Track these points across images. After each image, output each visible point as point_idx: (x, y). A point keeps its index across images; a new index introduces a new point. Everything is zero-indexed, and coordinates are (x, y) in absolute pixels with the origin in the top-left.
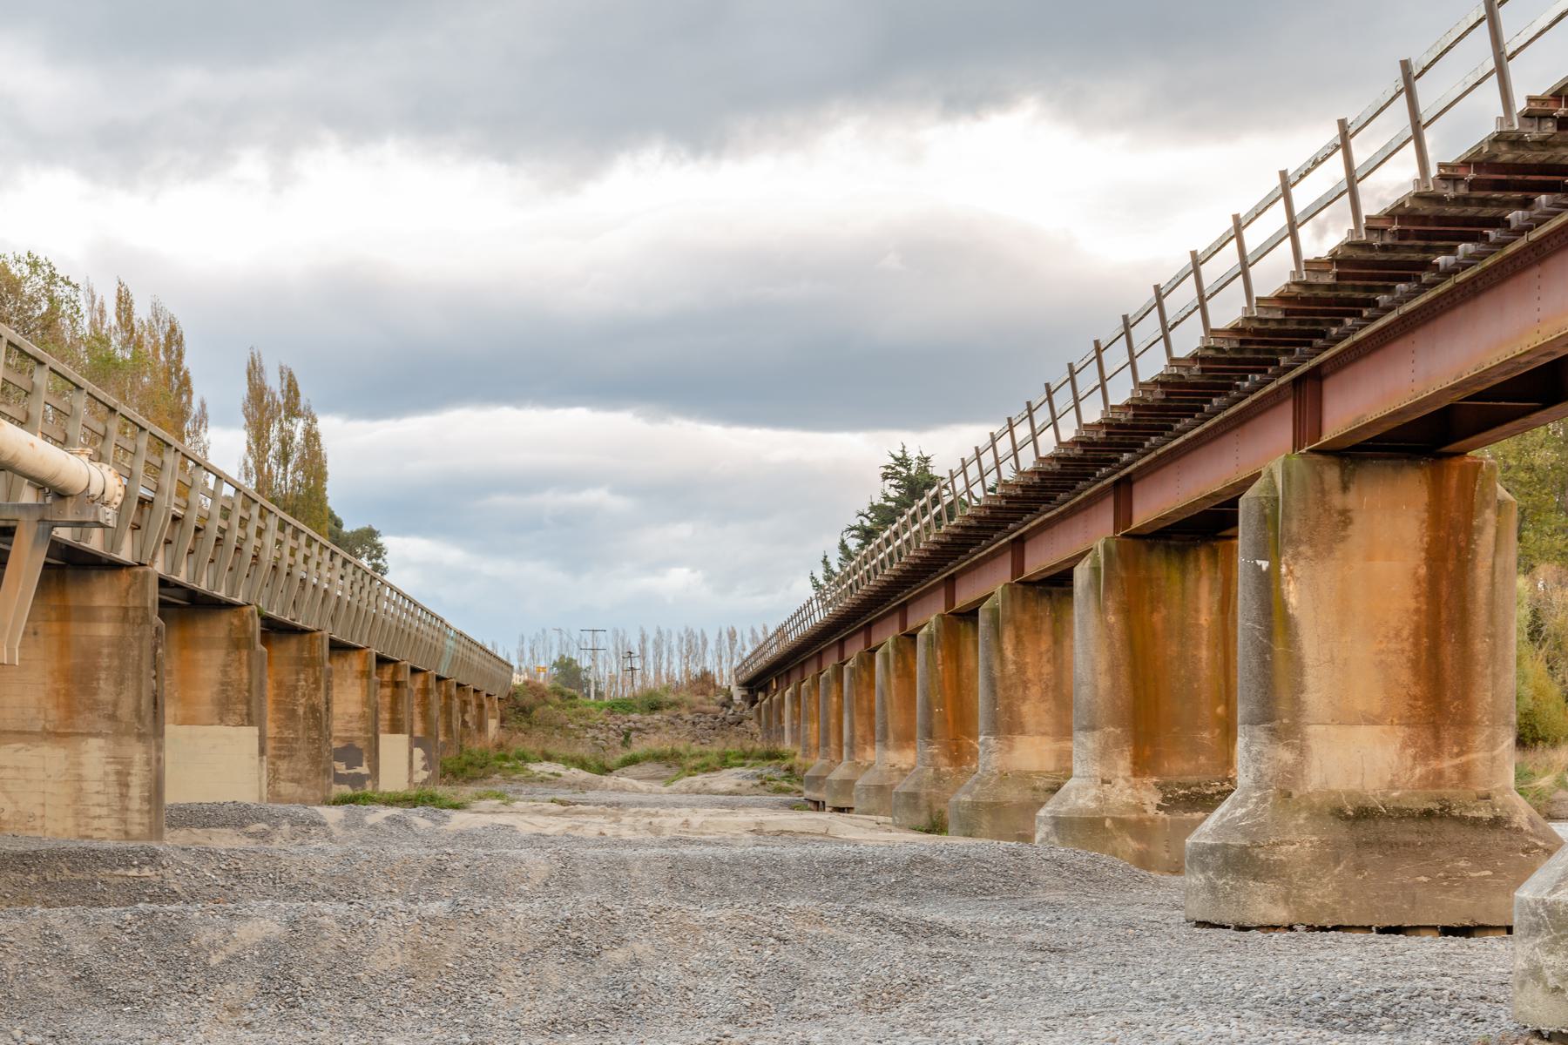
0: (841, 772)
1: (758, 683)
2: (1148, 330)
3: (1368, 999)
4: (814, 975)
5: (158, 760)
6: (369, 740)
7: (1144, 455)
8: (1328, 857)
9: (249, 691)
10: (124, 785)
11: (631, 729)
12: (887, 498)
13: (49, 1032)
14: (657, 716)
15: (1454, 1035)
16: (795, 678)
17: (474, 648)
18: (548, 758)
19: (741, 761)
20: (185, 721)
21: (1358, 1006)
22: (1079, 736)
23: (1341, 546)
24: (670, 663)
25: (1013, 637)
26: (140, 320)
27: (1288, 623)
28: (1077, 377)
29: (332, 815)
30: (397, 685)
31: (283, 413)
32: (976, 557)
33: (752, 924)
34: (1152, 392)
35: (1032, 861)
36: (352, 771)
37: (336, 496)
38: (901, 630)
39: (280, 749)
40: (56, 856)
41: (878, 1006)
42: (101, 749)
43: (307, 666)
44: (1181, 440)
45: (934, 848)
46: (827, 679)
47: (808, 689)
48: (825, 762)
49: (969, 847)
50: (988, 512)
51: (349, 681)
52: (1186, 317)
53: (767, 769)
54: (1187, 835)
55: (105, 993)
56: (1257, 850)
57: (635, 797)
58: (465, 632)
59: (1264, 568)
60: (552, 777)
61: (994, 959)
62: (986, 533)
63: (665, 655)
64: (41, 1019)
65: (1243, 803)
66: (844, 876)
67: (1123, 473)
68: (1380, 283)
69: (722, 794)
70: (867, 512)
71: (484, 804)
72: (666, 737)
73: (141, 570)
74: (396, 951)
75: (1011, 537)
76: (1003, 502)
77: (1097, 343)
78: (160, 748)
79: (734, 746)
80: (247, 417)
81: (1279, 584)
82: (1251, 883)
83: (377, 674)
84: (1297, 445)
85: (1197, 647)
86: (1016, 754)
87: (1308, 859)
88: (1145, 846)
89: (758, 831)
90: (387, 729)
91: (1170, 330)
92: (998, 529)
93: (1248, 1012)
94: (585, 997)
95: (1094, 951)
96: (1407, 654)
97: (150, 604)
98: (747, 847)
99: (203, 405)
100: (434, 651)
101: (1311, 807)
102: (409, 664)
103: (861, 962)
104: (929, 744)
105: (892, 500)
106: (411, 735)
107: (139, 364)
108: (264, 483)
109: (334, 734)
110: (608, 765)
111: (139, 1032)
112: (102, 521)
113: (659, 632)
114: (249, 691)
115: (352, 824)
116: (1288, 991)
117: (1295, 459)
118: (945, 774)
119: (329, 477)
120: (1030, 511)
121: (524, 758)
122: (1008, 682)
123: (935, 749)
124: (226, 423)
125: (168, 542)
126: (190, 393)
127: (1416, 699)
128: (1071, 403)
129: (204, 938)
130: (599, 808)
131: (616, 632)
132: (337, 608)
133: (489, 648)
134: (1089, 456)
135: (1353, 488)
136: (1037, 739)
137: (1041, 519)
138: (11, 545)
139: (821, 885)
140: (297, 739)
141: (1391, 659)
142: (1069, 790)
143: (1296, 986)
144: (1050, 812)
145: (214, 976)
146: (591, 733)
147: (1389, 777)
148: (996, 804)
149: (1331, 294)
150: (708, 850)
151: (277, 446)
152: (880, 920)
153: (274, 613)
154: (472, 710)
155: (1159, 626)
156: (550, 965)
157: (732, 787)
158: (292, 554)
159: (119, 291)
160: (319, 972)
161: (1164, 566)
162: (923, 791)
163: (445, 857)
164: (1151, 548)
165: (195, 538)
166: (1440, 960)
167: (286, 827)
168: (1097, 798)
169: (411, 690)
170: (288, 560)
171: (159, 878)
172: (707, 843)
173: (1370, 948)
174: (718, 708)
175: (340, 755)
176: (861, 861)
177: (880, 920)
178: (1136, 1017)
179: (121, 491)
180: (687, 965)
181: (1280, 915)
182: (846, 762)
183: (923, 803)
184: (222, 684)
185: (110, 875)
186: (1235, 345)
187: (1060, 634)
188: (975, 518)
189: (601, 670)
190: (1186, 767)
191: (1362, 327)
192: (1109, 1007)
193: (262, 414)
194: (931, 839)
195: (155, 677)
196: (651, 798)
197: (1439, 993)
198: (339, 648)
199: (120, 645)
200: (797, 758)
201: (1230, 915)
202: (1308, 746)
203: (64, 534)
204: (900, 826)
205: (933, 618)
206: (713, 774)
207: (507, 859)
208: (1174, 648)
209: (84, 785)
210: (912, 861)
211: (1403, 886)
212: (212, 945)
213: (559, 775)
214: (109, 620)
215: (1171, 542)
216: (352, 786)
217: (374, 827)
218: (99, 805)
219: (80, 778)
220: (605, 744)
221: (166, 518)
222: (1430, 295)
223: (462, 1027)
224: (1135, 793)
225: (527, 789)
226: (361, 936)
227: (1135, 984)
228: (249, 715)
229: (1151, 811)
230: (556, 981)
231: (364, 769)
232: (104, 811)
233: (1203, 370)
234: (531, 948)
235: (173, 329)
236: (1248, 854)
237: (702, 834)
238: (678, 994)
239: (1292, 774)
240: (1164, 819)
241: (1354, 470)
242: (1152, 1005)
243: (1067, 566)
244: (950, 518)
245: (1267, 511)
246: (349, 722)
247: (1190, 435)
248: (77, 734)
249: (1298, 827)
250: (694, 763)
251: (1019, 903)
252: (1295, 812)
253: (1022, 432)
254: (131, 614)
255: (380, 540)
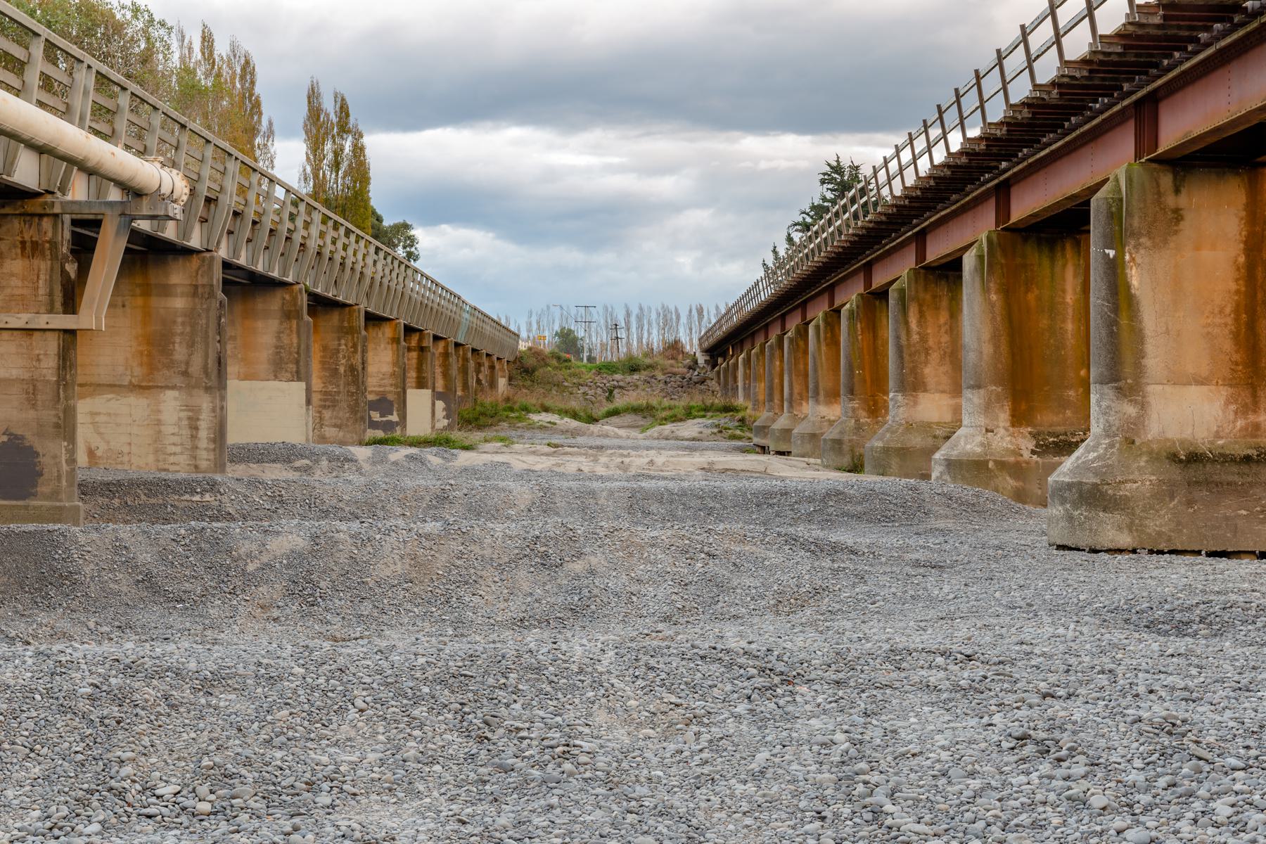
0: (782, 422)
1: (719, 349)
2: (1016, 60)
3: (1189, 609)
4: (736, 583)
5: (222, 408)
6: (398, 394)
7: (1018, 163)
8: (1165, 492)
9: (298, 353)
10: (195, 428)
11: (615, 387)
12: (824, 199)
13: (117, 623)
14: (636, 376)
15: (1258, 639)
16: (747, 346)
17: (486, 319)
18: (546, 410)
19: (702, 413)
20: (247, 377)
21: (1180, 615)
22: (968, 394)
23: (1174, 238)
24: (649, 334)
25: (916, 312)
26: (220, 55)
27: (1131, 302)
28: (962, 100)
29: (362, 453)
30: (422, 349)
31: (335, 130)
32: (887, 247)
33: (687, 542)
34: (1021, 112)
35: (927, 495)
36: (384, 419)
37: (378, 198)
38: (830, 307)
39: (325, 400)
40: (134, 484)
41: (786, 609)
42: (176, 399)
43: (347, 333)
44: (1047, 151)
45: (846, 484)
46: (771, 347)
47: (757, 355)
48: (771, 414)
49: (875, 483)
50: (895, 210)
51: (382, 346)
52: (1046, 51)
53: (723, 420)
54: (1049, 475)
55: (162, 593)
56: (1106, 487)
57: (616, 442)
58: (478, 307)
59: (1111, 256)
60: (549, 425)
61: (885, 573)
62: (895, 227)
63: (646, 327)
64: (111, 613)
65: (1095, 448)
66: (771, 505)
67: (1001, 178)
68: (1200, 24)
69: (687, 440)
70: (808, 210)
71: (488, 446)
72: (643, 393)
73: (208, 255)
74: (397, 561)
75: (914, 231)
76: (907, 202)
77: (977, 72)
78: (223, 398)
79: (697, 401)
80: (306, 132)
81: (1124, 268)
82: (1101, 514)
83: (405, 340)
84: (1138, 155)
85: (1064, 321)
86: (920, 408)
87: (1148, 495)
88: (1021, 483)
89: (708, 469)
90: (414, 385)
91: (1034, 61)
92: (903, 224)
93: (1087, 618)
94: (549, 599)
95: (968, 567)
96: (1229, 327)
97: (215, 282)
98: (698, 481)
99: (271, 124)
100: (453, 322)
101: (1150, 453)
102: (432, 333)
103: (775, 574)
104: (851, 400)
105: (828, 201)
106: (433, 390)
107: (219, 90)
108: (319, 186)
109: (369, 389)
110: (595, 416)
111: (188, 624)
112: (171, 214)
113: (641, 309)
114: (298, 353)
115: (375, 461)
116: (1123, 602)
117: (1136, 167)
118: (863, 424)
119: (372, 181)
120: (929, 209)
121: (526, 409)
122: (913, 349)
123: (855, 404)
124: (289, 134)
125: (230, 233)
126: (260, 114)
127: (1237, 364)
128: (958, 121)
129: (243, 550)
130: (582, 451)
131: (606, 308)
132: (371, 286)
133: (503, 322)
134: (974, 164)
135: (1184, 191)
136: (937, 396)
137: (938, 216)
138: (98, 233)
139: (752, 512)
140: (339, 393)
141: (1216, 331)
142: (959, 437)
143: (1130, 597)
144: (943, 455)
145: (250, 580)
146: (582, 389)
147: (1215, 429)
148: (903, 449)
149: (1160, 32)
150: (662, 483)
151: (330, 156)
152: (793, 540)
153: (319, 290)
154: (485, 370)
155: (1033, 303)
156: (522, 573)
157: (695, 434)
158: (334, 243)
159: (203, 32)
160: (334, 577)
161: (1036, 255)
162: (846, 438)
163: (448, 487)
164: (1025, 240)
165: (253, 229)
166: (1251, 578)
167: (324, 463)
168: (982, 444)
169: (434, 354)
170: (330, 247)
171: (217, 503)
172: (665, 478)
173: (1196, 568)
174: (685, 370)
175: (373, 406)
176: (786, 494)
177: (793, 540)
178: (993, 621)
179: (187, 191)
180: (633, 575)
181: (1125, 540)
182: (786, 414)
183: (846, 447)
184: (277, 347)
185: (178, 500)
186: (1085, 73)
187: (955, 313)
188: (885, 214)
189: (594, 339)
190: (1055, 419)
191: (1188, 59)
192: (975, 612)
193: (318, 131)
194: (853, 477)
195: (219, 341)
196: (629, 442)
197: (1248, 605)
198: (373, 319)
199: (191, 315)
200: (748, 411)
201: (1084, 540)
202: (1148, 402)
203: (144, 225)
204: (827, 467)
205: (854, 297)
206: (679, 424)
207: (498, 489)
208: (1045, 322)
209: (163, 428)
210: (827, 494)
211: (1227, 518)
212: (249, 555)
213: (555, 424)
214: (182, 295)
215: (1042, 235)
216: (384, 431)
217: (396, 463)
218: (174, 444)
219: (159, 423)
220: (594, 399)
221: (228, 213)
222: (1241, 33)
223: (448, 623)
224: (1014, 440)
225: (528, 434)
226: (370, 549)
227: (998, 595)
228: (298, 372)
229: (1026, 455)
230: (526, 587)
231: (394, 418)
232: (178, 449)
233: (1061, 94)
234: (507, 560)
235: (247, 62)
236: (1099, 490)
237: (662, 471)
238: (624, 597)
239: (1135, 424)
240: (1037, 462)
241: (1185, 176)
242: (1009, 611)
243: (958, 255)
244: (866, 214)
245: (1114, 209)
246: (382, 379)
247: (1054, 147)
248: (157, 387)
249: (1139, 468)
250: (664, 414)
251: (915, 528)
252: (1137, 456)
253: (920, 144)
254: (200, 290)
255: (412, 232)
